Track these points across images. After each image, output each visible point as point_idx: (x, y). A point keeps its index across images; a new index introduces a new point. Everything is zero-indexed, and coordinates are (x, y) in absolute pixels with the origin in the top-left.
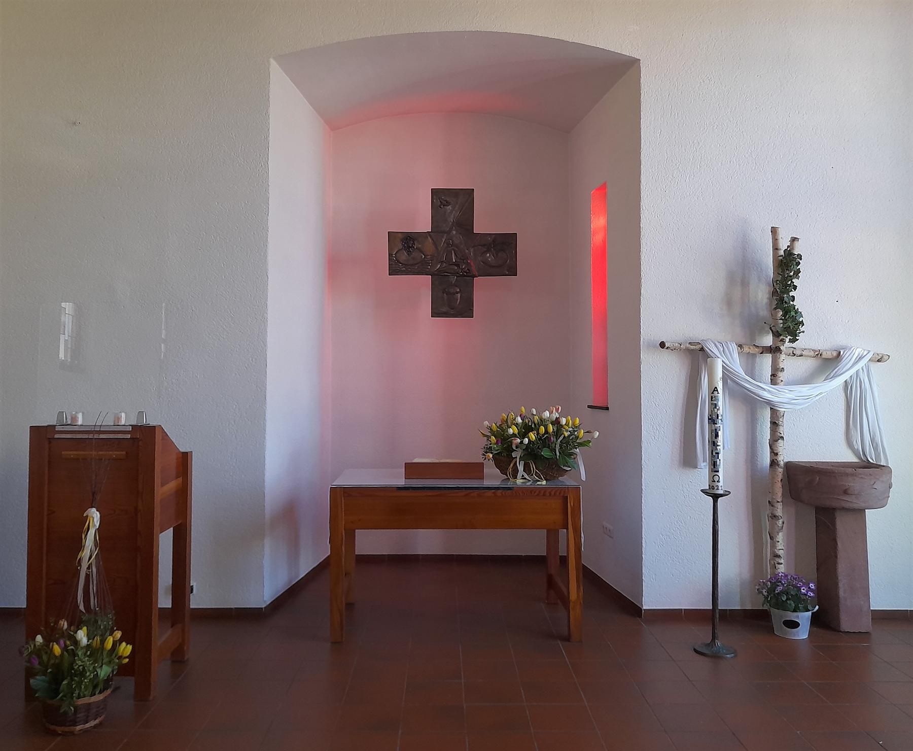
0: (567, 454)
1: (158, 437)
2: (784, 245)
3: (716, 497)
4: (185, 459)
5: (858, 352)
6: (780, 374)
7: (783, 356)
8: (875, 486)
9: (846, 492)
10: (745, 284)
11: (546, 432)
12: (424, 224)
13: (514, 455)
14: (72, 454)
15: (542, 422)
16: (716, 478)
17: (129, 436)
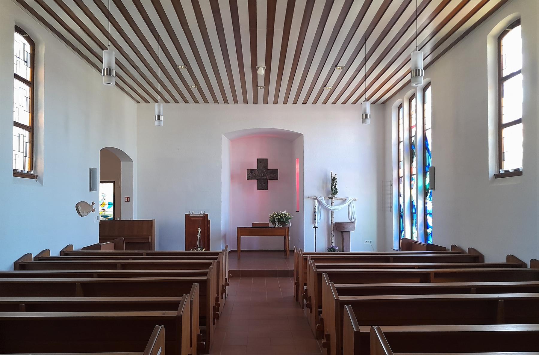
0: (287, 220)
2: (333, 176)
3: (315, 228)
5: (351, 198)
6: (333, 203)
7: (333, 199)
9: (344, 228)
10: (326, 183)
11: (282, 216)
12: (255, 167)
13: (276, 221)
14: (193, 219)
15: (282, 214)
17: (203, 216)
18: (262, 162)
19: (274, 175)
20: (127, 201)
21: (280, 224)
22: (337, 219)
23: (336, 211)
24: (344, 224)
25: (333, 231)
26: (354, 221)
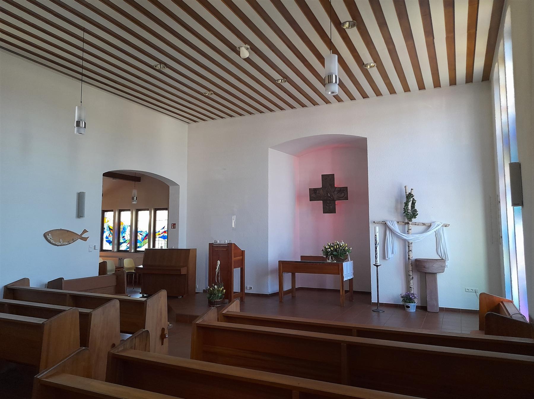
1: (233, 246)
2: (409, 191)
3: (377, 266)
4: (243, 253)
7: (410, 225)
8: (434, 265)
9: (424, 267)
16: (376, 261)
17: (227, 245)
18: (328, 179)
19: (343, 193)
20: (174, 228)
21: (333, 258)
22: (415, 255)
23: (415, 242)
24: (424, 262)
25: (411, 272)
26: (446, 259)
